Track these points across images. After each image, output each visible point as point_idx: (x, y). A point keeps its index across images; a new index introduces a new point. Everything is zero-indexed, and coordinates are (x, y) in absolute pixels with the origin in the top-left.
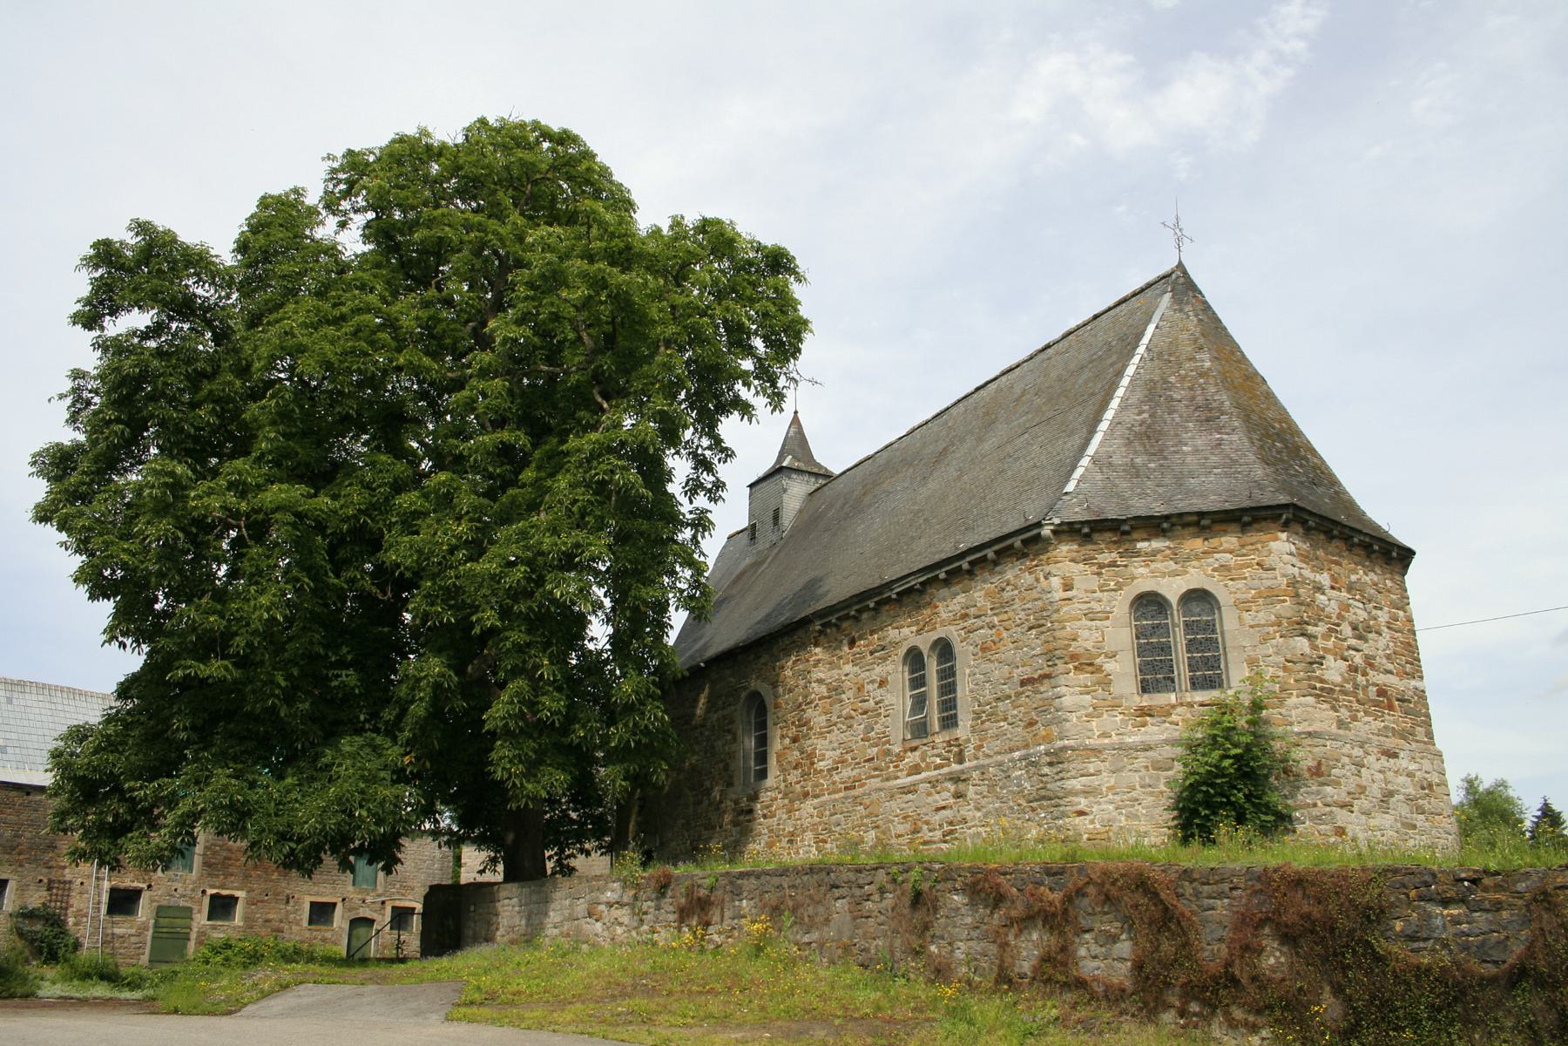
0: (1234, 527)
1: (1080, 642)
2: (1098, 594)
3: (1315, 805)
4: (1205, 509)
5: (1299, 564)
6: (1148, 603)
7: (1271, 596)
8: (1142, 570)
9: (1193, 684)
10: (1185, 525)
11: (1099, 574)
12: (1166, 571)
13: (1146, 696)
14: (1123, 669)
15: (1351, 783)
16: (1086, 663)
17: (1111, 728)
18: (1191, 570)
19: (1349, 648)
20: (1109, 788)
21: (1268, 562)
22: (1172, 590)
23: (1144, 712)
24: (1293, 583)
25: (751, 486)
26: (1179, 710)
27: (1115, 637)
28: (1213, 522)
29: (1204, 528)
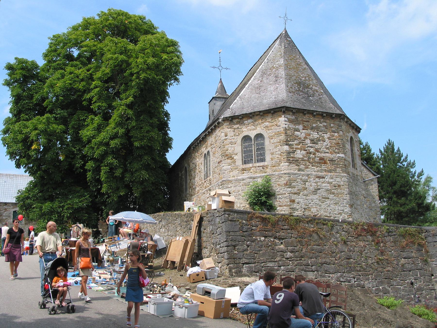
0: (270, 115)
1: (229, 151)
2: (234, 137)
3: (285, 194)
4: (261, 110)
5: (288, 124)
6: (246, 138)
7: (278, 134)
8: (245, 129)
9: (258, 161)
10: (257, 115)
11: (234, 131)
12: (251, 130)
13: (244, 165)
14: (238, 158)
15: (301, 186)
16: (230, 157)
17: (235, 175)
18: (258, 128)
19: (308, 147)
20: (233, 191)
21: (279, 124)
22: (252, 134)
23: (243, 170)
24: (286, 129)
25: (209, 103)
26: (252, 168)
27: (237, 149)
28: (264, 113)
29: (261, 116)
